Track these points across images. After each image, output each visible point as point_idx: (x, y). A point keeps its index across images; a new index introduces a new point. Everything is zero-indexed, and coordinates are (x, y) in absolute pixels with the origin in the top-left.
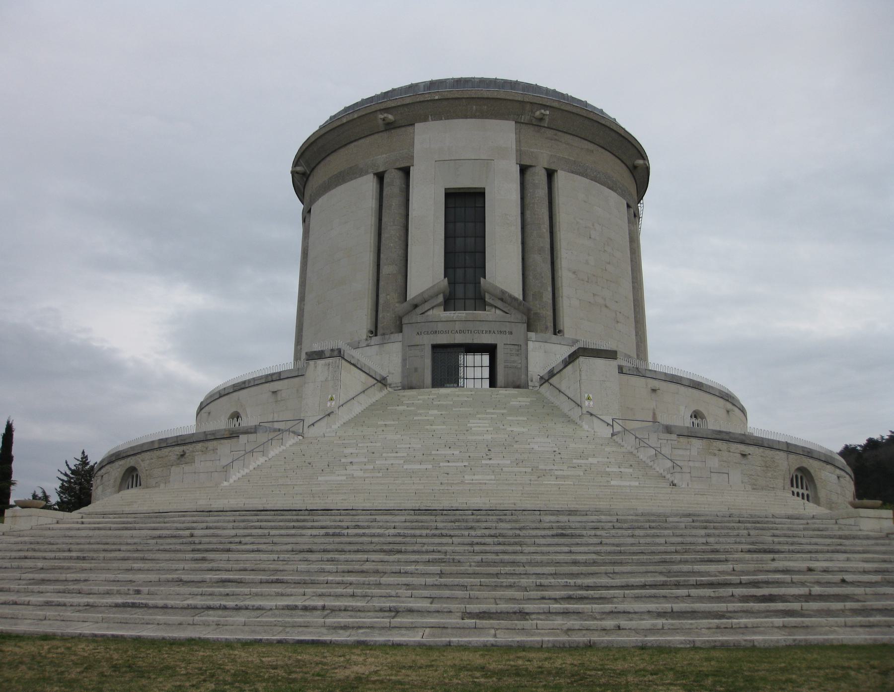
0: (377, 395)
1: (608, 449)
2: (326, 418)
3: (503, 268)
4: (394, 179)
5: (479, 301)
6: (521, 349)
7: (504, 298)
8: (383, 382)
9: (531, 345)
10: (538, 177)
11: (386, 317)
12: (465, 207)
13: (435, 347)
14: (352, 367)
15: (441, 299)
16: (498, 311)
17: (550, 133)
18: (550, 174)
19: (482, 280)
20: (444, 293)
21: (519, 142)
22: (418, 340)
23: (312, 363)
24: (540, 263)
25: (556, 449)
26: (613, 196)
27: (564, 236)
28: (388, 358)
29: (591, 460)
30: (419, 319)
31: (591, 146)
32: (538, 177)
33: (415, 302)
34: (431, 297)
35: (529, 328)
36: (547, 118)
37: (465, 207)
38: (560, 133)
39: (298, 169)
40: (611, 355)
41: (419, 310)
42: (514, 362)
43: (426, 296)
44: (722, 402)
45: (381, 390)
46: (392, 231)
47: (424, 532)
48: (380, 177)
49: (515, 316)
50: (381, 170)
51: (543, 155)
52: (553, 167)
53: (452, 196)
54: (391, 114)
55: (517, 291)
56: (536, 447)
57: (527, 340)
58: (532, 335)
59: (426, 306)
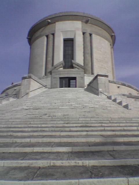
0: (44, 89)
1: (106, 100)
2: (26, 95)
3: (79, 58)
4: (51, 37)
5: (72, 67)
6: (83, 78)
7: (78, 65)
8: (45, 86)
9: (85, 77)
10: (88, 35)
11: (49, 70)
12: (69, 43)
13: (60, 78)
14: (35, 82)
15: (62, 65)
16: (77, 69)
17: (90, 25)
18: (91, 35)
19: (73, 61)
20: (63, 64)
21: (82, 27)
22: (56, 76)
23: (23, 80)
24: (89, 58)
25: (90, 100)
26: (107, 42)
27: (94, 50)
28: (48, 81)
29: (101, 103)
30: (56, 71)
31: (101, 29)
32: (88, 35)
33: (55, 67)
34: (59, 65)
35: (85, 73)
36: (90, 21)
37: (69, 43)
38: (93, 25)
39: (28, 37)
40: (107, 76)
41: (56, 69)
42: (81, 81)
43: (58, 65)
44: (136, 91)
45: (45, 89)
46: (50, 49)
47: (30, 129)
48: (47, 36)
49: (83, 70)
50: (47, 34)
51: (89, 29)
52: (91, 33)
53: (66, 41)
54: (50, 20)
55: (82, 64)
56: (84, 100)
57: (84, 76)
58: (85, 75)
59: (58, 68)
